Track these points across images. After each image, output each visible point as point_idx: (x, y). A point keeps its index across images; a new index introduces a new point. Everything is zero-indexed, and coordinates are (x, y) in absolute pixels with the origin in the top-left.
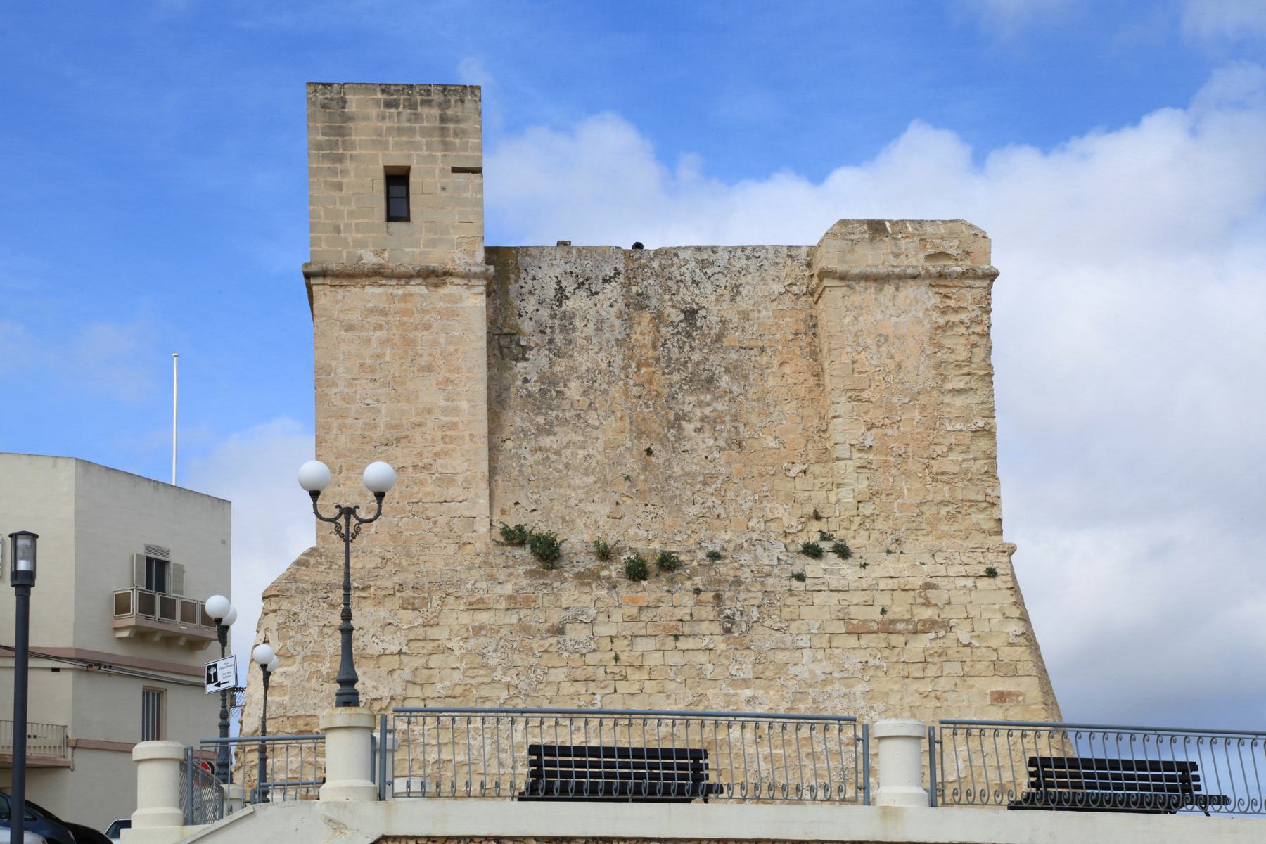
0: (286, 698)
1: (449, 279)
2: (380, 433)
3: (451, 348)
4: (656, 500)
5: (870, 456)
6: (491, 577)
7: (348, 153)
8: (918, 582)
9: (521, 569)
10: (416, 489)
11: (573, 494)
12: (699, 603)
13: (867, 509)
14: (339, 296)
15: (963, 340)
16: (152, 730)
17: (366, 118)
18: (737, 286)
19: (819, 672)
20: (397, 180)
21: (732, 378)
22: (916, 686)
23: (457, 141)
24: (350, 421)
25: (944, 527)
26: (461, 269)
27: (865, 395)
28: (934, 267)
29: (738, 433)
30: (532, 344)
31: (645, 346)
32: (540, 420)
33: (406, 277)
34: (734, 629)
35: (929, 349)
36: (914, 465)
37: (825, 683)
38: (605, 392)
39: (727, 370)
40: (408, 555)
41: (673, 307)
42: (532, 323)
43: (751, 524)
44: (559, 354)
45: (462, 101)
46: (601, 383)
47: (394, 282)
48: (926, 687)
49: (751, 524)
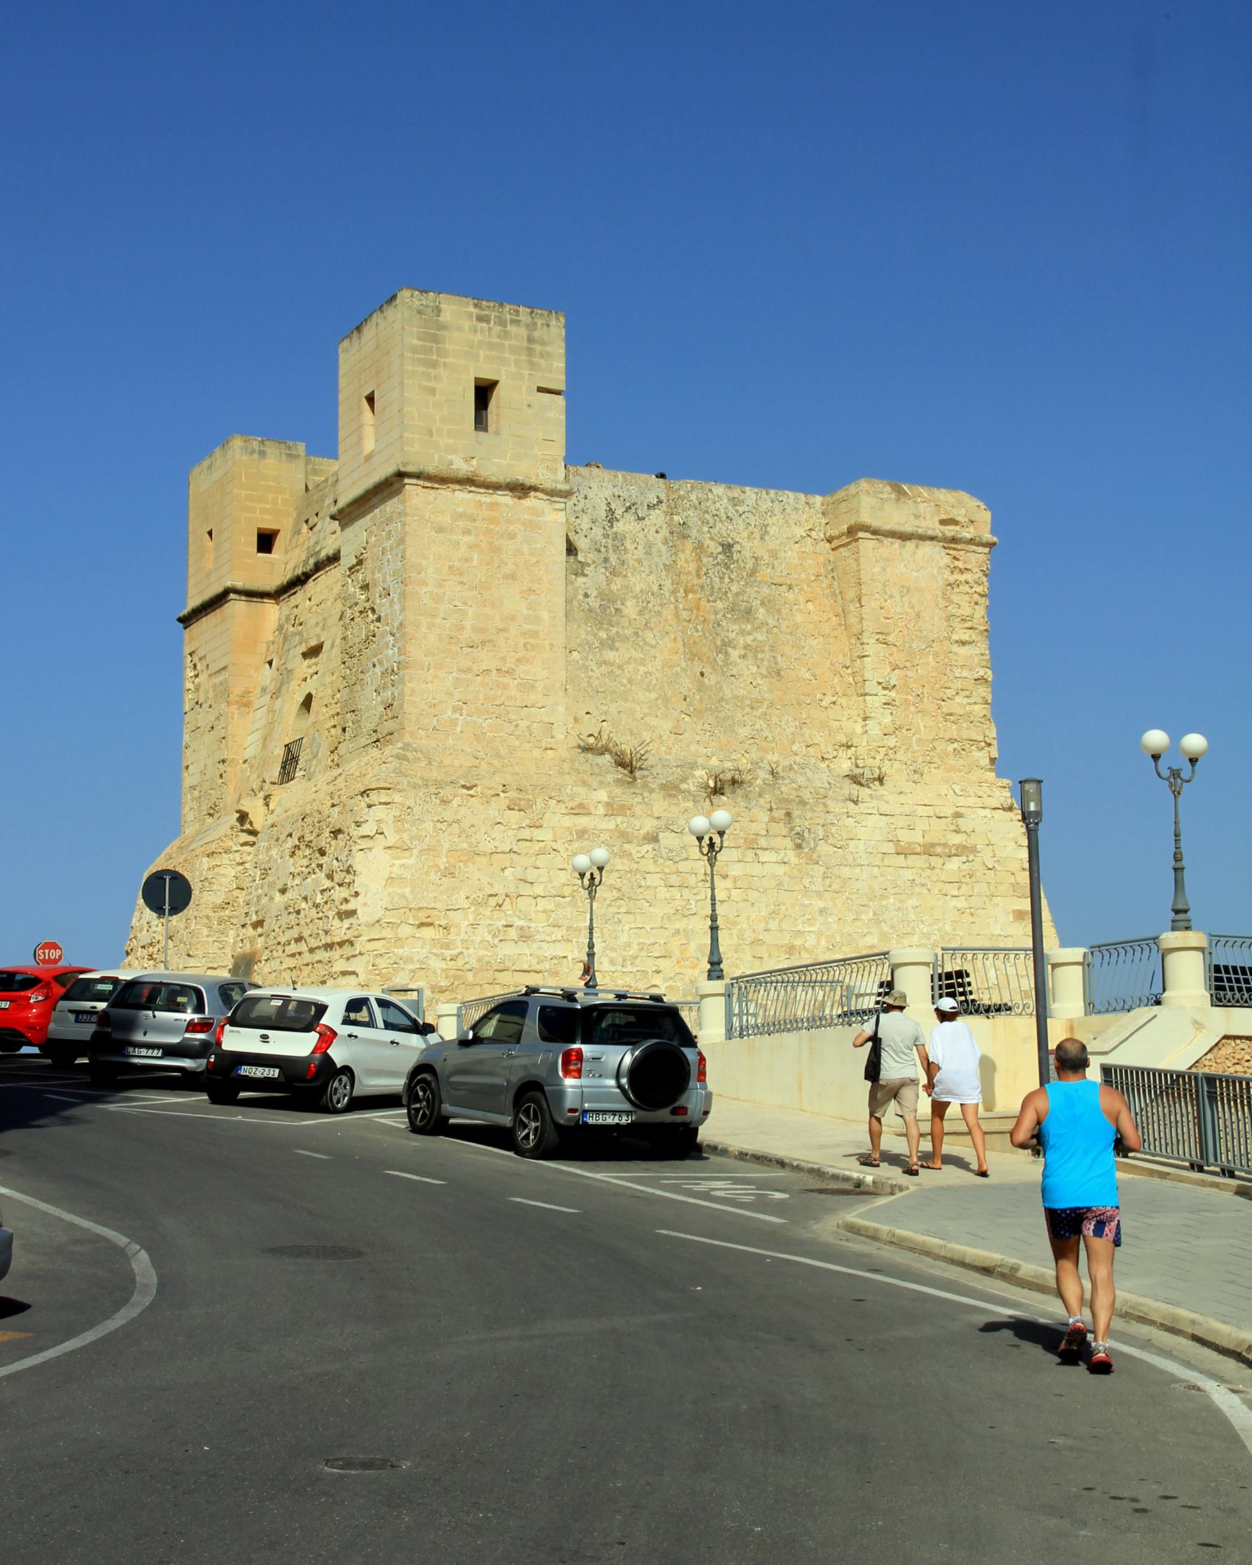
0: (407, 890)
1: (532, 494)
2: (468, 634)
3: (534, 559)
4: (711, 719)
5: (893, 694)
6: (584, 783)
7: (442, 360)
8: (949, 811)
9: (610, 778)
10: (500, 692)
11: (638, 709)
12: (773, 820)
13: (891, 741)
14: (431, 498)
15: (967, 598)
16: (1181, 918)
17: (460, 329)
18: (766, 526)
19: (876, 888)
20: (484, 392)
21: (768, 611)
22: (953, 903)
23: (542, 362)
24: (438, 621)
25: (951, 761)
26: (548, 485)
27: (891, 639)
28: (950, 531)
29: (776, 663)
30: (589, 561)
31: (689, 573)
32: (603, 635)
33: (496, 487)
34: (804, 845)
35: (942, 603)
36: (928, 705)
37: (883, 897)
38: (659, 613)
39: (763, 603)
40: (498, 756)
41: (712, 539)
42: (588, 540)
43: (795, 748)
44: (613, 573)
45: (548, 326)
46: (654, 604)
47: (482, 490)
48: (961, 903)
49: (795, 748)
